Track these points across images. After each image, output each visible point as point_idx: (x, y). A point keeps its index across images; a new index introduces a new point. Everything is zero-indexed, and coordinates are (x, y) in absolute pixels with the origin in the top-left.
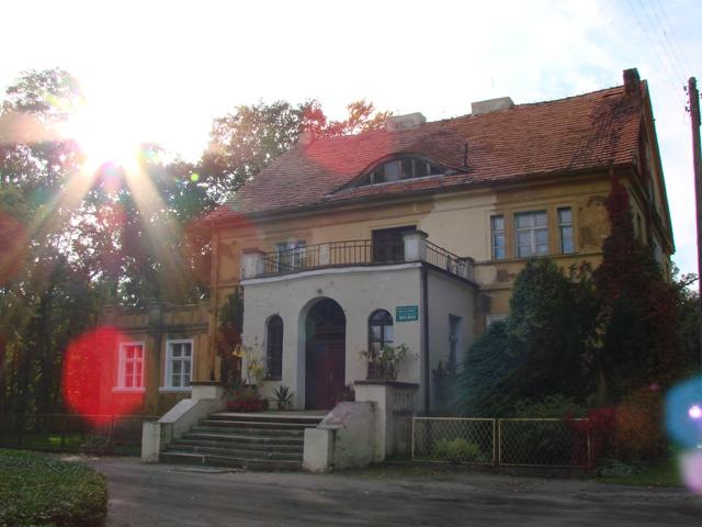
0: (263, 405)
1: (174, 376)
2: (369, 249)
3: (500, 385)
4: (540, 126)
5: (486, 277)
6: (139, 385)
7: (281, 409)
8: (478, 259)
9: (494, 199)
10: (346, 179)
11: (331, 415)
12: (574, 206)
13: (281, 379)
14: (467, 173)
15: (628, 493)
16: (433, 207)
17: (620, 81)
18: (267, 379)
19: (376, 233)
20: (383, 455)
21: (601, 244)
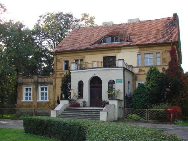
0: (78, 105)
1: (26, 97)
2: (102, 63)
3: (144, 100)
4: (149, 28)
5: (136, 71)
6: (46, 99)
7: (84, 106)
8: (134, 66)
9: (138, 49)
10: (94, 42)
11: (105, 108)
12: (161, 53)
13: (83, 98)
14: (130, 42)
15: (184, 127)
16: (121, 51)
17: (172, 16)
18: (78, 98)
19: (104, 58)
20: (117, 119)
21: (168, 63)
